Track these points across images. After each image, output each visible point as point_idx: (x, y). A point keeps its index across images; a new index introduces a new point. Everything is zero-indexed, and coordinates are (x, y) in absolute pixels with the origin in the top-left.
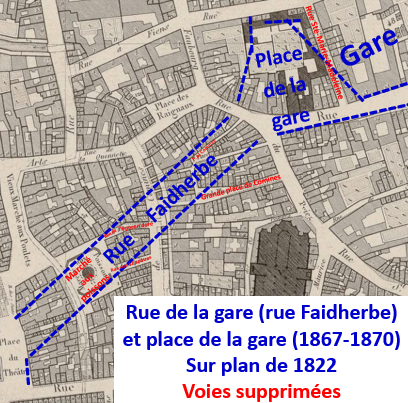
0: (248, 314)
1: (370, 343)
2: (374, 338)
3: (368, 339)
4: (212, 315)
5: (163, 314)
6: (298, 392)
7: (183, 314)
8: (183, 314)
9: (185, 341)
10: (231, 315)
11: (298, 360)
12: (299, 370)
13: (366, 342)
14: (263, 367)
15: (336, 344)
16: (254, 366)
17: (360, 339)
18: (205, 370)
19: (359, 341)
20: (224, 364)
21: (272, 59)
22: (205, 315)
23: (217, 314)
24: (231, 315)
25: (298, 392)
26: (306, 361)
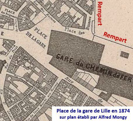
0: (91, 111)
1: (124, 112)
2: (125, 111)
3: (123, 111)
4: (82, 111)
5: (69, 111)
6: (112, 37)
7: (74, 111)
8: (74, 111)
9: (67, 111)
10: (87, 111)
11: (120, 110)
12: (120, 112)
13: (123, 112)
14: (77, 117)
15: (125, 112)
16: (116, 111)
17: (121, 111)
18: (64, 118)
19: (121, 111)
20: (68, 117)
21: (61, 111)
22: (80, 111)
23: (83, 111)
24: (87, 111)
25: (112, 37)
26: (122, 110)
